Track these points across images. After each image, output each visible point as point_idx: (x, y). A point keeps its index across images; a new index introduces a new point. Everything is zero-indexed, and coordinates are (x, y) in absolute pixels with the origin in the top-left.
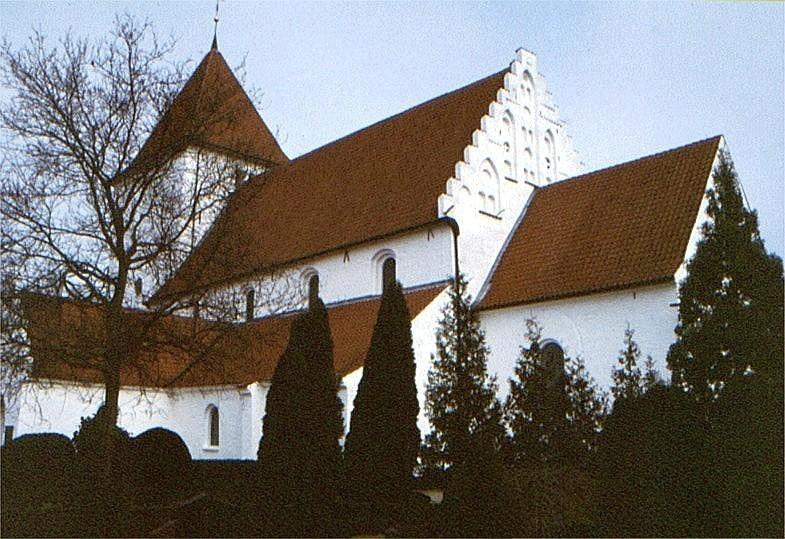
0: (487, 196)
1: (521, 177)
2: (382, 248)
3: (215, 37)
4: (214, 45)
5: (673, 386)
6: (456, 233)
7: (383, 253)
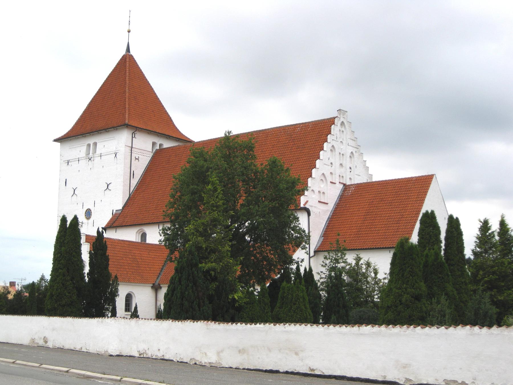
0: (322, 193)
1: (337, 182)
2: (140, 228)
3: (128, 42)
4: (128, 50)
5: (270, 277)
6: (309, 214)
7: (141, 230)
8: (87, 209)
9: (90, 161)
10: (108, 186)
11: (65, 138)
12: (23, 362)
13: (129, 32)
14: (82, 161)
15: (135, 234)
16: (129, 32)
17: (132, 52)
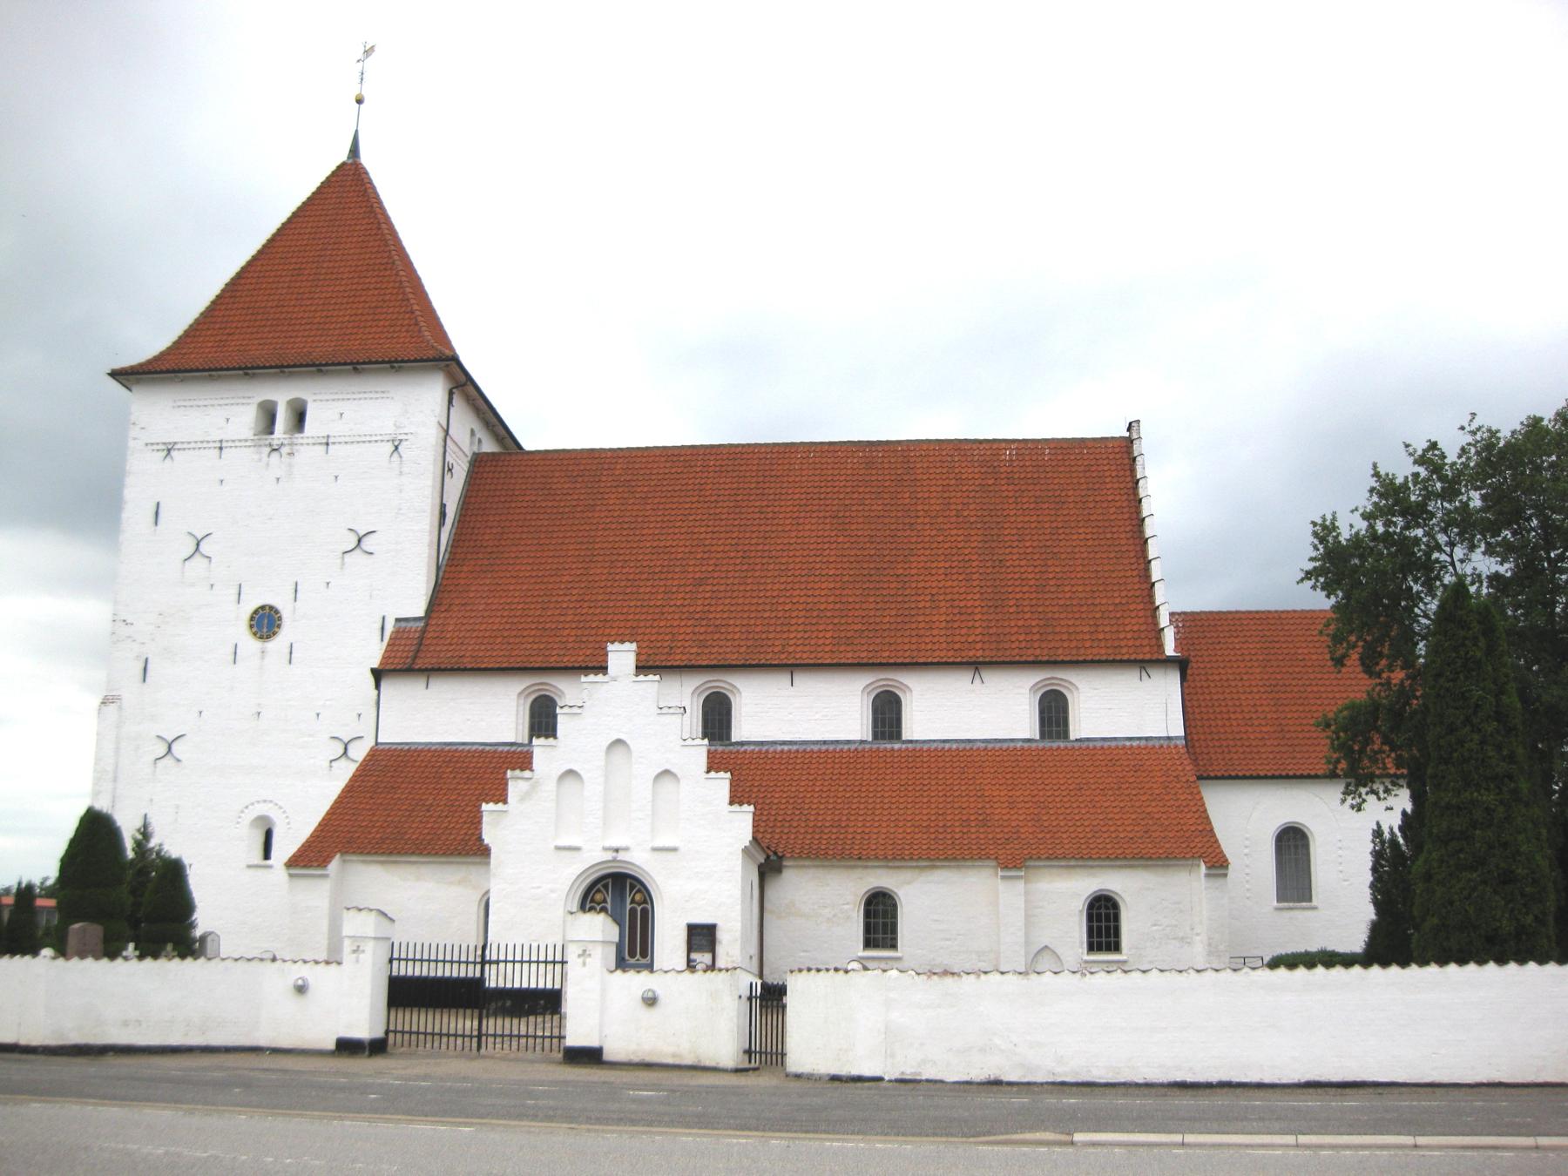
3: (357, 131)
4: (354, 151)
8: (263, 608)
9: (275, 455)
10: (198, 545)
11: (150, 372)
12: (1461, 1138)
13: (359, 101)
14: (336, 446)
15: (516, 697)
16: (359, 101)
17: (366, 160)
